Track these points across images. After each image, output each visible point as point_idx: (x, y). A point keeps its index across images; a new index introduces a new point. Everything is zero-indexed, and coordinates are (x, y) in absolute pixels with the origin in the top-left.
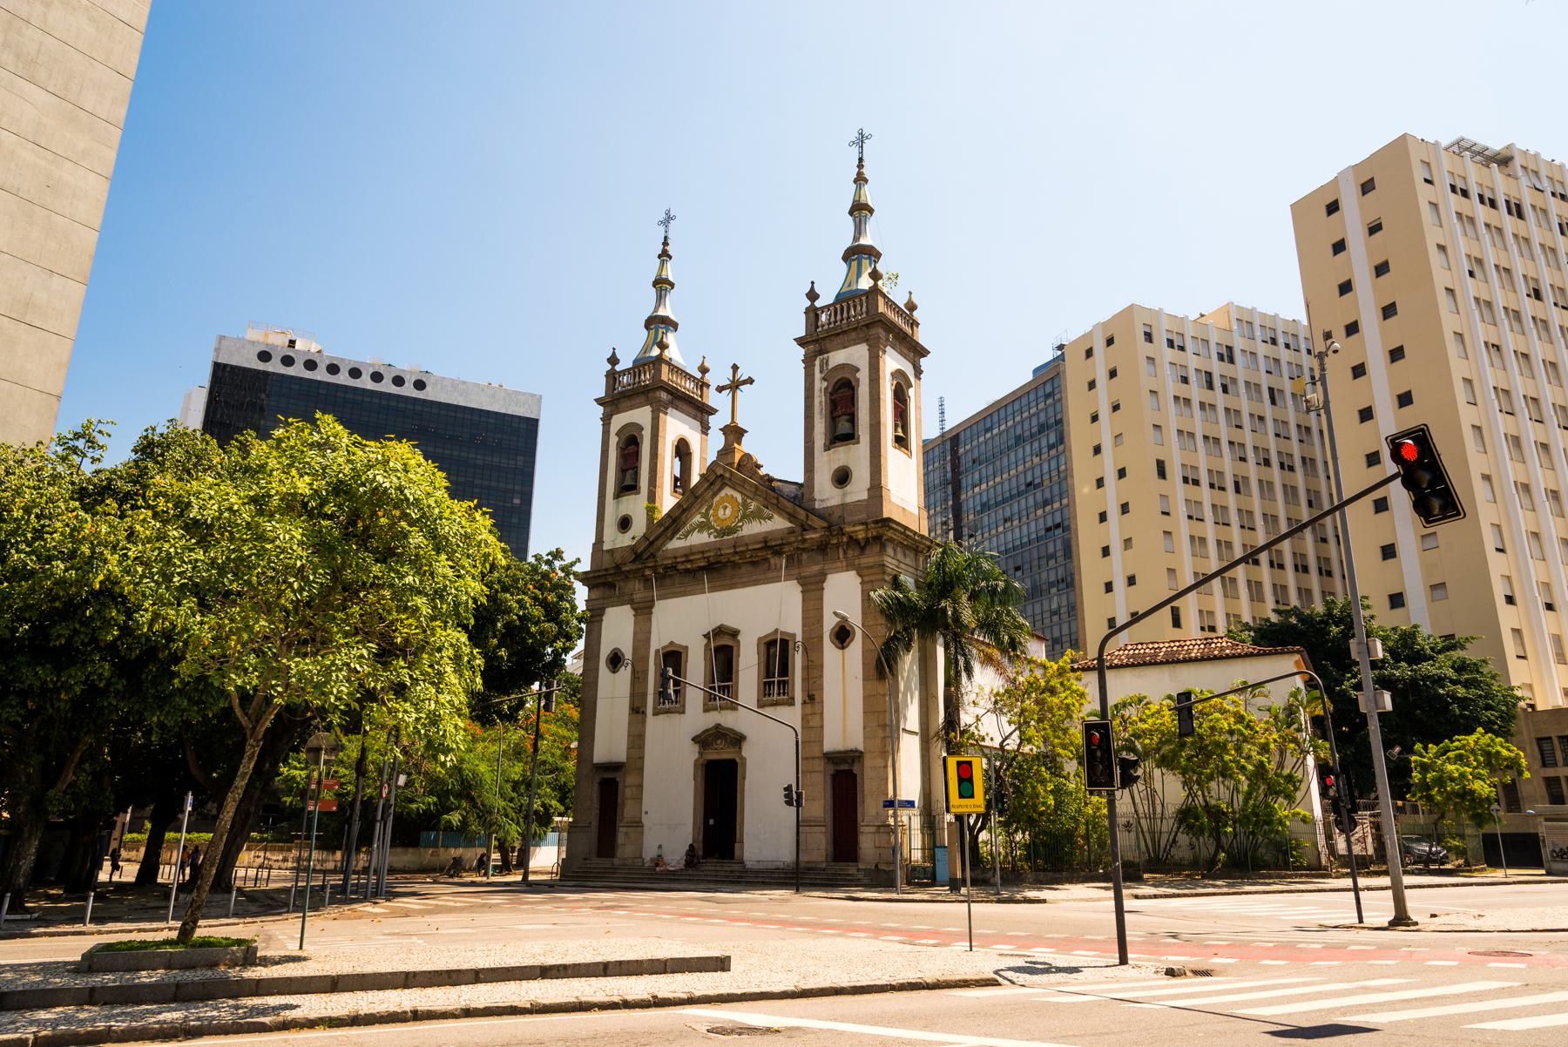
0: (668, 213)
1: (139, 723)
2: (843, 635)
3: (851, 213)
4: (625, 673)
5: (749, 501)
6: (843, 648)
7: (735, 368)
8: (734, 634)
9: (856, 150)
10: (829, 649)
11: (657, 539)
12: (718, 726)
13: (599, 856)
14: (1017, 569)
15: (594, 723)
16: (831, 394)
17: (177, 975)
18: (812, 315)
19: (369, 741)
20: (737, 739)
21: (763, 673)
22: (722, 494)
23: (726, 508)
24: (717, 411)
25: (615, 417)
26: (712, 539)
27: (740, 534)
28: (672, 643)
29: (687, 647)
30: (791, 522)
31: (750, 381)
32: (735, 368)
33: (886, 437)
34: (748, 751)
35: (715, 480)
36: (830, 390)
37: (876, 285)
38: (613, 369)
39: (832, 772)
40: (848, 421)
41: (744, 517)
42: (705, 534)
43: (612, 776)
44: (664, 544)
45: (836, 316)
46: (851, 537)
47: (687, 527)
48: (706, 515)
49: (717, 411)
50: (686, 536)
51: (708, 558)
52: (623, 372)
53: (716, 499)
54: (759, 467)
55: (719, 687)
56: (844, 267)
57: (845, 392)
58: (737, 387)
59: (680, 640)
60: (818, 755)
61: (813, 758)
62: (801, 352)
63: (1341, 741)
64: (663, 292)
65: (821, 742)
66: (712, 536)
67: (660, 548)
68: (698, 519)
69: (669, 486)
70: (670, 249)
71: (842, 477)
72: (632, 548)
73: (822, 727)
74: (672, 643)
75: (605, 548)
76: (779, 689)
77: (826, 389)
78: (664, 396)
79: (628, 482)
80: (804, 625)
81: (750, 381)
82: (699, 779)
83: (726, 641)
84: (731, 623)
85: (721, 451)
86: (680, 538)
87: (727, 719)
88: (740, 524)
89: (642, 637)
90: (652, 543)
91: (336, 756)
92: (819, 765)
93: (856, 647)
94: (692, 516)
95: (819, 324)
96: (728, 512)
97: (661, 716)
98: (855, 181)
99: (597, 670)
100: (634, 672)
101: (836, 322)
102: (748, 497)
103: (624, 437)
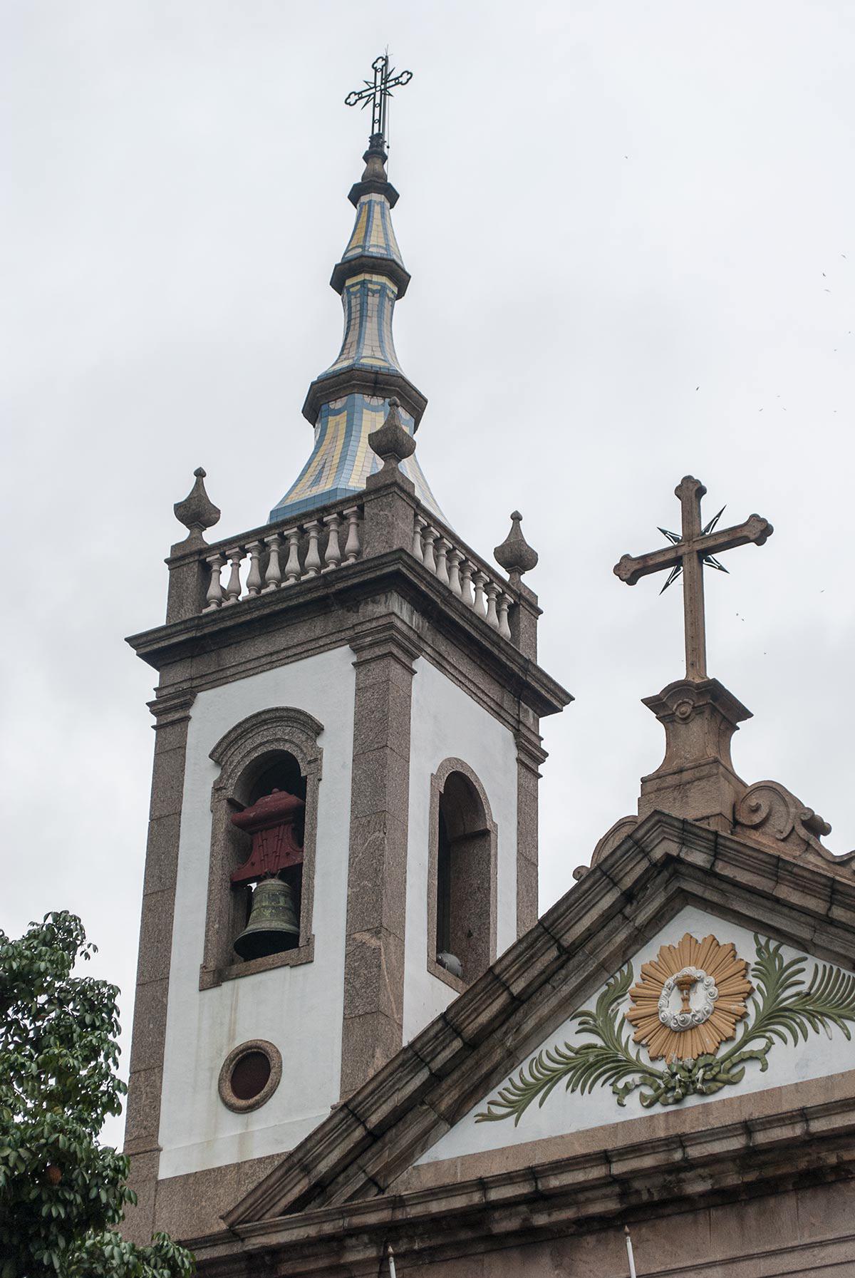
0: (382, 68)
3: (340, 279)
5: (788, 953)
7: (691, 492)
9: (363, 117)
11: (398, 1116)
18: (191, 574)
22: (671, 935)
23: (687, 985)
25: (203, 698)
26: (634, 1108)
27: (753, 1080)
31: (757, 531)
32: (691, 492)
35: (642, 884)
37: (390, 471)
38: (195, 538)
41: (774, 1016)
42: (602, 1094)
44: (424, 1141)
45: (302, 554)
47: (523, 1072)
48: (601, 1024)
51: (623, 1181)
52: (235, 547)
53: (644, 958)
54: (817, 827)
56: (308, 433)
58: (704, 555)
62: (148, 679)
64: (373, 301)
66: (633, 1100)
67: (406, 1158)
69: (423, 939)
70: (394, 173)
72: (298, 1160)
75: (165, 1172)
78: (400, 610)
79: (266, 920)
81: (757, 531)
85: (658, 776)
86: (489, 1117)
88: (757, 1045)
90: (375, 1136)
94: (544, 1029)
95: (213, 591)
96: (700, 1001)
98: (356, 195)
102: (786, 938)
103: (241, 759)
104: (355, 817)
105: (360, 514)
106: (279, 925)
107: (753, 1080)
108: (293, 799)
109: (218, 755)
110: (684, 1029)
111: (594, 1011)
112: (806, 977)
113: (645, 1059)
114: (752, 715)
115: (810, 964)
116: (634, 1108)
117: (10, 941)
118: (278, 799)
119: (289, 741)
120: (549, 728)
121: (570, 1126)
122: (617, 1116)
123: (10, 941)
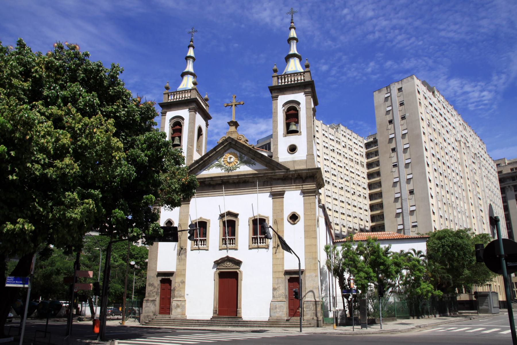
1: (70, 67)
2: (294, 218)
5: (243, 155)
8: (236, 215)
12: (227, 257)
13: (160, 313)
15: (157, 252)
16: (286, 112)
20: (238, 263)
21: (222, 235)
30: (266, 166)
34: (242, 268)
36: (286, 110)
39: (289, 278)
43: (168, 277)
55: (228, 239)
57: (292, 112)
59: (205, 217)
60: (281, 270)
61: (279, 272)
63: (225, 262)
65: (283, 265)
71: (293, 149)
73: (283, 258)
74: (201, 218)
76: (260, 240)
77: (284, 110)
80: (274, 213)
82: (216, 280)
87: (232, 254)
88: (239, 166)
91: (447, 295)
92: (282, 275)
97: (253, 250)
102: (243, 153)
104: (189, 131)
105: (190, 92)
106: (178, 143)
107: (238, 170)
108: (180, 127)
109: (171, 120)
110: (230, 163)
111: (295, 36)
112: (245, 158)
113: (225, 166)
114: (269, 87)
115: (246, 157)
116: (223, 171)
117: (303, 93)
118: (178, 127)
119: (180, 120)
120: (209, 122)
121: (215, 172)
122: (222, 172)
123: (303, 93)
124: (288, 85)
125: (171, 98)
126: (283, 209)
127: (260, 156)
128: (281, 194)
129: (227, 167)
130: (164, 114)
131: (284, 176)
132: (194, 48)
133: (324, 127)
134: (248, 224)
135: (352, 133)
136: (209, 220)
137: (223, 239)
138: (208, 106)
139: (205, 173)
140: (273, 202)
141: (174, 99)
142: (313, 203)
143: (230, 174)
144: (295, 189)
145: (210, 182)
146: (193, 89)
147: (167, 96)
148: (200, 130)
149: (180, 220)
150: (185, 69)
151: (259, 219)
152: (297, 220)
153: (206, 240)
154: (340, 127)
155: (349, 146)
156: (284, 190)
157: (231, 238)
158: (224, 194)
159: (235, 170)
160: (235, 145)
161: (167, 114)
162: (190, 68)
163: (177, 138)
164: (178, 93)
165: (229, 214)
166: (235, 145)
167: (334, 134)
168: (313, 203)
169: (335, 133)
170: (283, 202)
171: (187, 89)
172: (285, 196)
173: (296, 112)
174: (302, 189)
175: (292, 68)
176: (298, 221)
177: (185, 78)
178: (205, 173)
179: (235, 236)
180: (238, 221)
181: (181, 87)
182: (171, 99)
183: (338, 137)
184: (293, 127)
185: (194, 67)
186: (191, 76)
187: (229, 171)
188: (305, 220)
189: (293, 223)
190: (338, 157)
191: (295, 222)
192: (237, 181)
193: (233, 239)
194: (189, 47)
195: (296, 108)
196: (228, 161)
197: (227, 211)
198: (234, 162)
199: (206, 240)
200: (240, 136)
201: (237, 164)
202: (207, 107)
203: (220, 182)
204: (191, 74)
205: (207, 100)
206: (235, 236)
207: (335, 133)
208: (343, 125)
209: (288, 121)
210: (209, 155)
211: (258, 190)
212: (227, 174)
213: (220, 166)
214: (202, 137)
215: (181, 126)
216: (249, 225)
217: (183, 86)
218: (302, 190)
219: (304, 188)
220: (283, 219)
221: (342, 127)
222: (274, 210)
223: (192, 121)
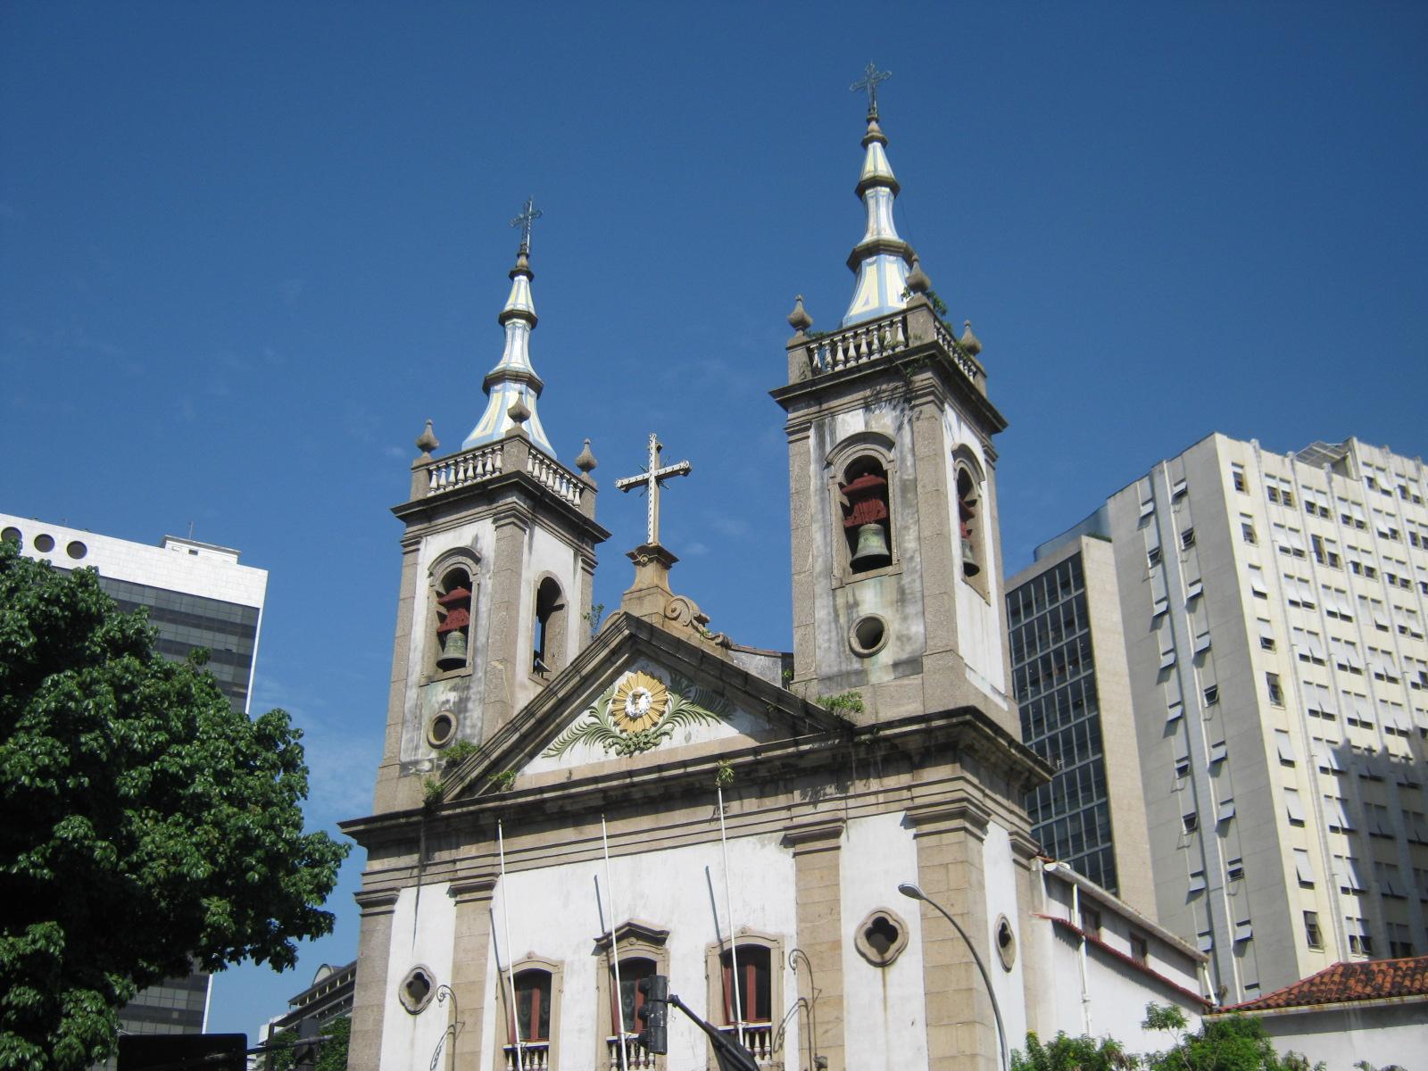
2: (882, 933)
4: (437, 1013)
6: (883, 965)
8: (657, 938)
10: (857, 973)
14: (822, 877)
17: (368, 827)
19: (906, 580)
24: (607, 535)
28: (530, 957)
29: (562, 963)
33: (994, 541)
40: (876, 533)
46: (894, 747)
49: (607, 535)
50: (560, 751)
54: (221, 971)
55: (745, 1030)
57: (867, 480)
68: (585, 718)
83: (640, 950)
84: (649, 919)
88: (668, 727)
89: (469, 951)
93: (910, 964)
99: (381, 1007)
100: (455, 1010)
101: (847, 360)
102: (683, 675)
103: (442, 572)
105: (502, 449)
110: (634, 718)
113: (617, 730)
118: (460, 592)
119: (466, 563)
124: (858, 368)
125: (447, 477)
126: (838, 901)
127: (738, 682)
128: (831, 832)
129: (624, 735)
130: (412, 544)
131: (834, 757)
132: (530, 277)
133: (1272, 461)
134: (704, 975)
135: (1418, 469)
136: (559, 965)
137: (610, 1044)
138: (984, 376)
139: (541, 770)
140: (799, 870)
141: (835, 363)
142: (957, 862)
143: (641, 760)
144: (882, 808)
145: (560, 803)
146: (510, 438)
147: (423, 474)
148: (548, 596)
149: (457, 969)
150: (497, 363)
151: (740, 950)
152: (894, 947)
153: (546, 1048)
154: (1352, 450)
155: (1414, 528)
156: (842, 814)
157: (757, 1029)
158: (724, 834)
159: (656, 745)
160: (649, 643)
161: (422, 546)
162: (516, 354)
163: (456, 634)
164: (849, 335)
165: (632, 931)
166: (649, 643)
167: (1325, 488)
168: (957, 862)
169: (1330, 481)
170: (837, 867)
171: (886, 313)
172: (496, 892)
173: (880, 480)
174: (908, 804)
175: (867, 303)
176: (900, 951)
177: (870, 270)
178: (541, 770)
179: (770, 1020)
180: (666, 960)
181: (478, 435)
182: (449, 483)
183: (1351, 497)
184: (872, 544)
185: (534, 351)
186: (892, 258)
187: (631, 753)
188: (927, 941)
189: (876, 958)
190: (1361, 584)
191: (888, 955)
192: (662, 791)
193: (763, 1033)
194: (513, 275)
195: (879, 465)
196: (631, 709)
197: (622, 920)
198: (650, 713)
199: (546, 1048)
200: (673, 606)
201: (661, 721)
202: (979, 377)
203: (600, 803)
204: (517, 377)
205: (972, 350)
206: (770, 1020)
207: (1330, 481)
208: (1362, 439)
209: (849, 524)
210: (555, 694)
211: (723, 824)
212: (625, 764)
213: (601, 733)
214: (565, 619)
215: (468, 586)
216: (707, 977)
217: (485, 429)
218: (908, 809)
219: (918, 802)
220: (837, 945)
221: (1362, 451)
222: (802, 905)
223: (512, 562)
